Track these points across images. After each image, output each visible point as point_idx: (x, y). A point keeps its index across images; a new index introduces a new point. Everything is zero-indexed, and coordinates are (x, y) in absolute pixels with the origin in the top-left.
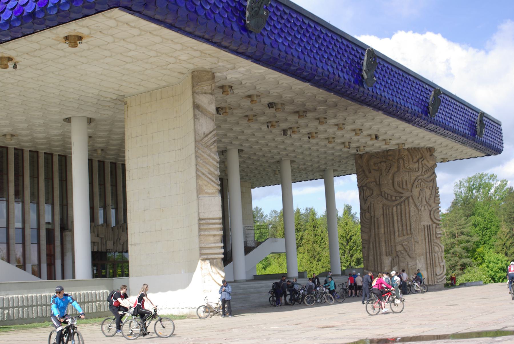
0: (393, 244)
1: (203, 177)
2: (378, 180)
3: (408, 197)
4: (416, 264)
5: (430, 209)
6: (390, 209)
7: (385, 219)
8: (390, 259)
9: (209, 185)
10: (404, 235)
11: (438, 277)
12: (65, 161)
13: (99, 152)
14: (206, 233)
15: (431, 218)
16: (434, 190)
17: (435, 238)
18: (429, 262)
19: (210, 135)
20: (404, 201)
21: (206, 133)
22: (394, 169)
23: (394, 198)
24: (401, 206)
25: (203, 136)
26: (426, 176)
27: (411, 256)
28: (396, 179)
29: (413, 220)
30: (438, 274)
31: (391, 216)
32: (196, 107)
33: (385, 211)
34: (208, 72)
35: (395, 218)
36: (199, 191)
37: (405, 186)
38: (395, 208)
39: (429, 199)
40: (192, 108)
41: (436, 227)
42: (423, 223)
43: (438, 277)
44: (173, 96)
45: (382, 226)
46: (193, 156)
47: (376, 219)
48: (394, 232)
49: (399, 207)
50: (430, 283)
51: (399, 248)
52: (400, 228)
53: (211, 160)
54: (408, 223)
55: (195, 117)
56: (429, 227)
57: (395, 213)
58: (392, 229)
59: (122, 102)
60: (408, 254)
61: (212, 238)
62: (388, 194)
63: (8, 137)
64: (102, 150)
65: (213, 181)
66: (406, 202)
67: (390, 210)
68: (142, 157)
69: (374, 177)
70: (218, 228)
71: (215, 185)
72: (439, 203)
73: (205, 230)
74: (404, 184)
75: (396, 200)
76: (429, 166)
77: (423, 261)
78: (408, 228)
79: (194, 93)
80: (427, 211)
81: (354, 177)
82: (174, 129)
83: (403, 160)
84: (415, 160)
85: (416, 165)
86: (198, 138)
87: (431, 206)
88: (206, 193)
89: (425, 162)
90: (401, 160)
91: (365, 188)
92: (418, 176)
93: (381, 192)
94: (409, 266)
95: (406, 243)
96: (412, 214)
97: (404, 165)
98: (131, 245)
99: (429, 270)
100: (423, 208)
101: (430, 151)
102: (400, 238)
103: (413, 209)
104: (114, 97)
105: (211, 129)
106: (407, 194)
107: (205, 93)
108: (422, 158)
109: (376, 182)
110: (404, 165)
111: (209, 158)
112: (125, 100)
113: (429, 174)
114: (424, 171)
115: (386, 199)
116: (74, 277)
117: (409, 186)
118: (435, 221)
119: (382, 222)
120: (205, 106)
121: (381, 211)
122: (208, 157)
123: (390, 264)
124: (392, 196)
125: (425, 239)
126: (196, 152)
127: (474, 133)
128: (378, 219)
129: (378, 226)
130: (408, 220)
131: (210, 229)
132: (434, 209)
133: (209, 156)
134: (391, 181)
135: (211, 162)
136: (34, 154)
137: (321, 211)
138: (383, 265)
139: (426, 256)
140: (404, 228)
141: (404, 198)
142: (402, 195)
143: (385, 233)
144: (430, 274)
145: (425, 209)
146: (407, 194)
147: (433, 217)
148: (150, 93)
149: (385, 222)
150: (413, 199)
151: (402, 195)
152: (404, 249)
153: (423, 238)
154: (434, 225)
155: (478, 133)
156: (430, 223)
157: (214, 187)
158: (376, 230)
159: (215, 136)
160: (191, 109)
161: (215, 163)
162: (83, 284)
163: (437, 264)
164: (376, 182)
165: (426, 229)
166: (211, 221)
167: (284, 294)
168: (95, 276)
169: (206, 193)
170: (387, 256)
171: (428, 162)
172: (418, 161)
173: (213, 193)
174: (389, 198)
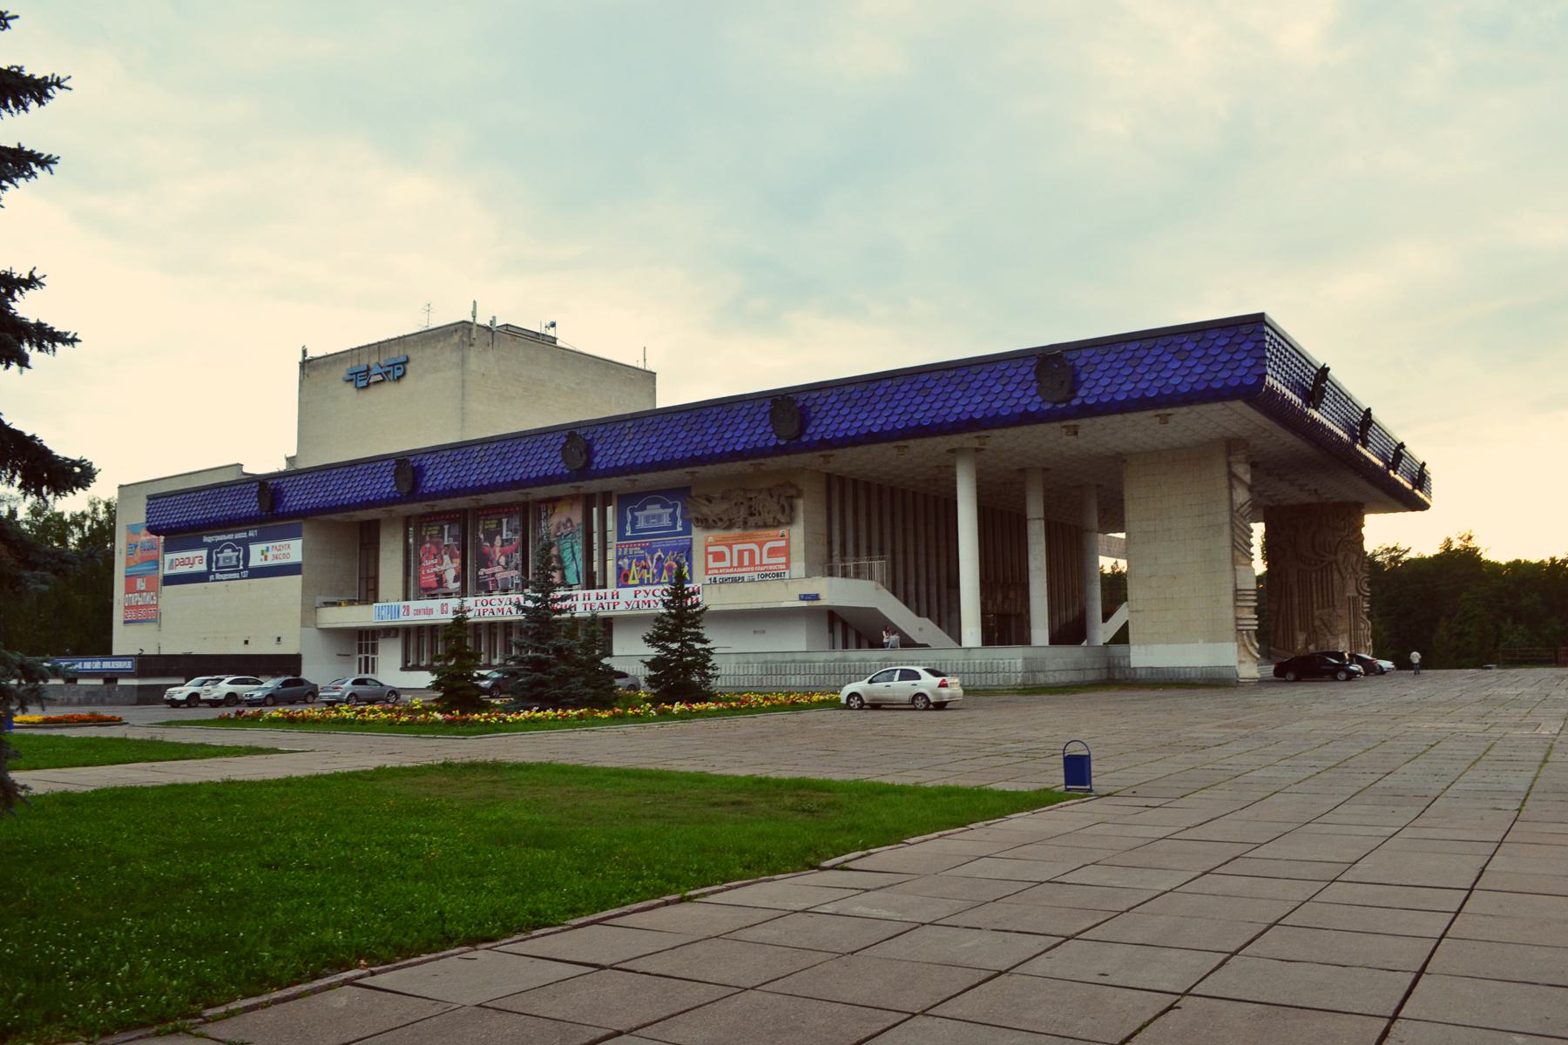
32: (1232, 476)
56: (1354, 599)
103: (1336, 576)
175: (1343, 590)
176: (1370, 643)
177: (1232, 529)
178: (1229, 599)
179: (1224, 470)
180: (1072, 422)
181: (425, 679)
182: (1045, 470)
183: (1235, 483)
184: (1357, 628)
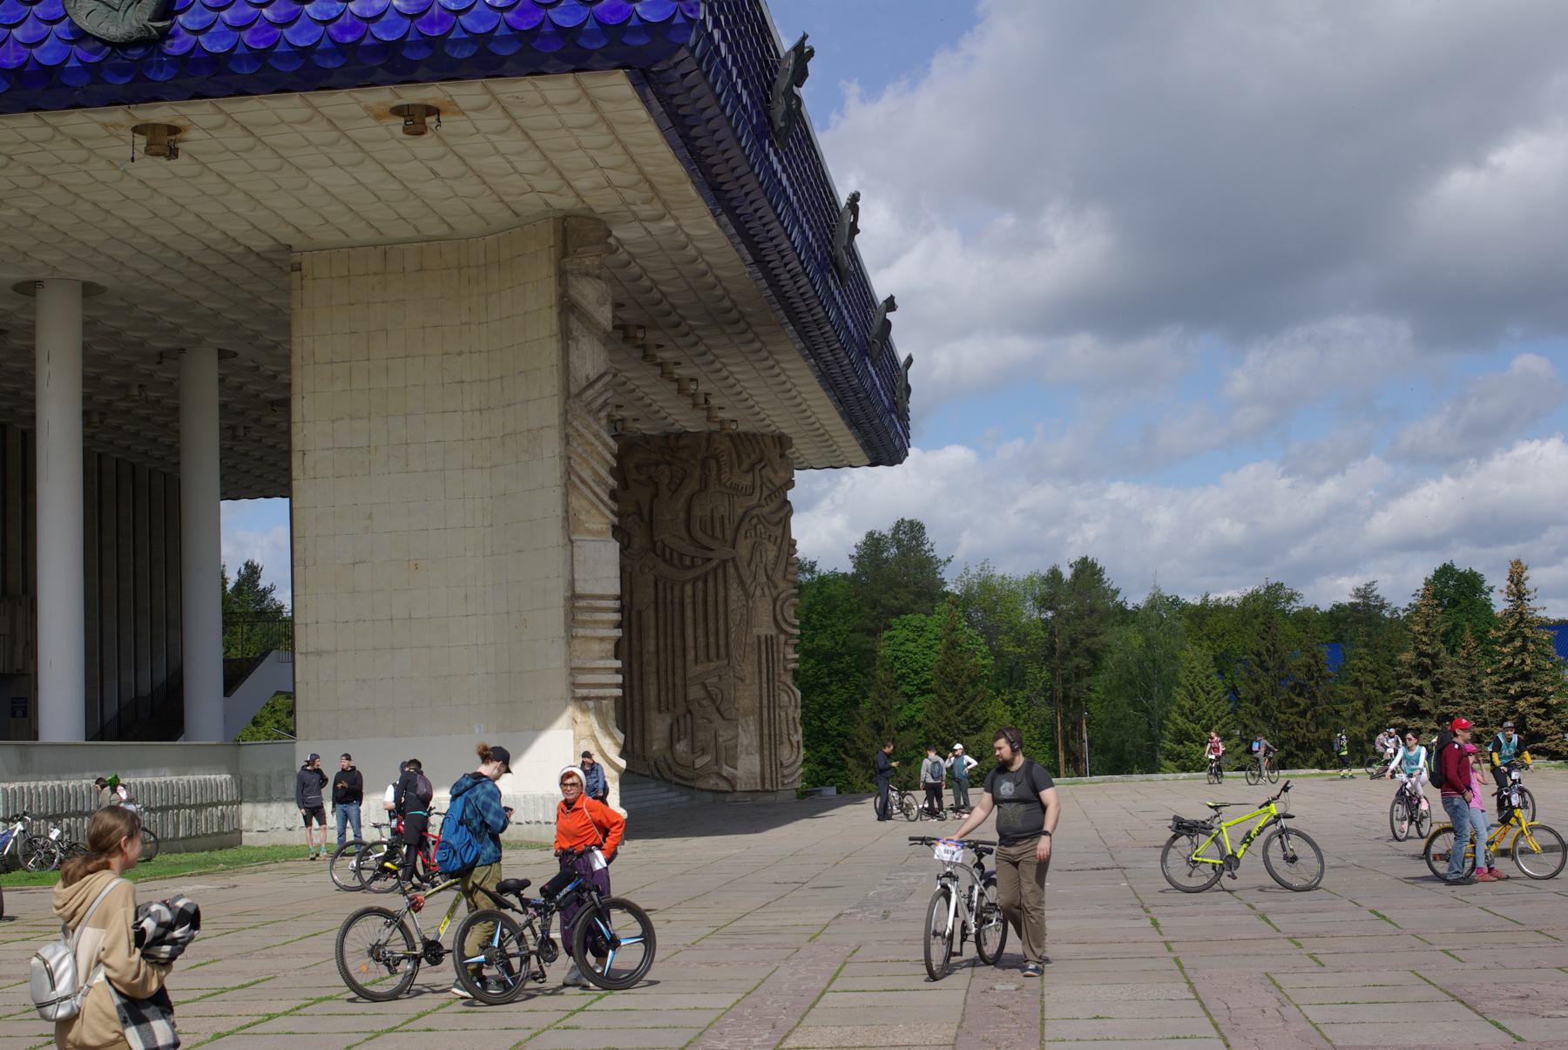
0: (679, 682)
1: (582, 486)
2: (646, 511)
3: (725, 562)
4: (737, 737)
5: (775, 593)
6: (677, 588)
7: (661, 615)
8: (668, 720)
9: (594, 511)
10: (708, 659)
14: (588, 632)
16: (785, 547)
18: (766, 731)
19: (599, 385)
20: (715, 569)
21: (593, 377)
22: (692, 485)
23: (687, 561)
24: (706, 582)
25: (584, 383)
26: (766, 510)
28: (697, 512)
29: (735, 618)
31: (677, 607)
32: (568, 307)
33: (661, 595)
34: (599, 221)
35: (689, 614)
36: (569, 522)
37: (718, 533)
38: (688, 589)
40: (555, 311)
42: (756, 631)
44: (459, 268)
45: (652, 633)
47: (634, 613)
48: (684, 649)
49: (700, 584)
50: (768, 786)
52: (701, 639)
53: (600, 448)
54: (722, 628)
56: (770, 641)
57: (688, 600)
58: (678, 642)
59: (283, 264)
60: (718, 710)
61: (596, 647)
62: (672, 550)
65: (601, 500)
66: (720, 572)
67: (677, 593)
68: (351, 418)
69: (637, 502)
70: (611, 622)
71: (607, 512)
73: (584, 624)
74: (717, 525)
75: (693, 566)
76: (778, 482)
77: (752, 728)
78: (722, 642)
80: (769, 599)
82: (460, 353)
83: (718, 463)
84: (745, 466)
85: (746, 481)
87: (776, 587)
88: (589, 532)
89: (768, 472)
90: (713, 463)
92: (749, 509)
93: (654, 544)
95: (715, 680)
96: (733, 606)
97: (719, 475)
98: (306, 654)
99: (766, 752)
100: (758, 593)
101: (782, 445)
102: (699, 667)
103: (735, 592)
104: (261, 244)
105: (602, 370)
106: (722, 552)
107: (587, 274)
108: (761, 460)
109: (640, 514)
110: (719, 475)
111: (597, 443)
112: (295, 258)
113: (773, 505)
114: (765, 494)
115: (665, 561)
117: (729, 533)
118: (785, 626)
119: (652, 623)
121: (651, 591)
122: (593, 440)
123: (667, 735)
124: (681, 556)
125: (760, 672)
128: (640, 612)
129: (640, 631)
130: (721, 621)
131: (595, 622)
133: (597, 436)
134: (682, 515)
135: (599, 454)
138: (647, 737)
139: (761, 715)
140: (712, 640)
141: (714, 563)
142: (710, 555)
143: (657, 651)
144: (767, 762)
145: (764, 595)
146: (722, 552)
147: (779, 617)
148: (384, 248)
149: (661, 624)
151: (710, 555)
152: (709, 695)
154: (782, 637)
156: (773, 632)
157: (603, 515)
158: (635, 642)
161: (609, 457)
162: (63, 759)
164: (640, 514)
169: (589, 532)
170: (660, 711)
171: (775, 472)
172: (751, 469)
173: (598, 533)
174: (676, 561)
175: (748, 622)
176: (798, 737)
177: (567, 439)
178: (557, 617)
179: (547, 291)
180: (161, 113)
181: (623, 813)
182: (90, 290)
183: (574, 323)
184: (773, 704)
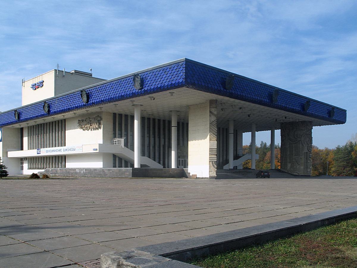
3: (299, 141)
5: (308, 145)
11: (308, 172)
12: (170, 122)
13: (182, 120)
15: (308, 149)
17: (309, 157)
20: (298, 142)
21: (213, 121)
25: (212, 122)
27: (298, 164)
30: (308, 171)
32: (210, 112)
39: (308, 142)
41: (310, 153)
43: (308, 172)
46: (209, 128)
50: (305, 174)
51: (294, 160)
55: (210, 116)
57: (294, 147)
63: (151, 115)
64: (183, 119)
72: (312, 143)
79: (210, 107)
81: (280, 130)
86: (210, 123)
91: (283, 136)
94: (297, 167)
100: (305, 145)
116: (65, 167)
120: (213, 112)
124: (293, 140)
126: (210, 127)
127: (330, 116)
132: (310, 146)
136: (159, 120)
137: (268, 144)
150: (301, 142)
153: (304, 157)
154: (309, 152)
155: (334, 116)
159: (216, 122)
160: (209, 113)
163: (308, 167)
165: (305, 153)
166: (225, 145)
167: (245, 173)
168: (132, 177)
